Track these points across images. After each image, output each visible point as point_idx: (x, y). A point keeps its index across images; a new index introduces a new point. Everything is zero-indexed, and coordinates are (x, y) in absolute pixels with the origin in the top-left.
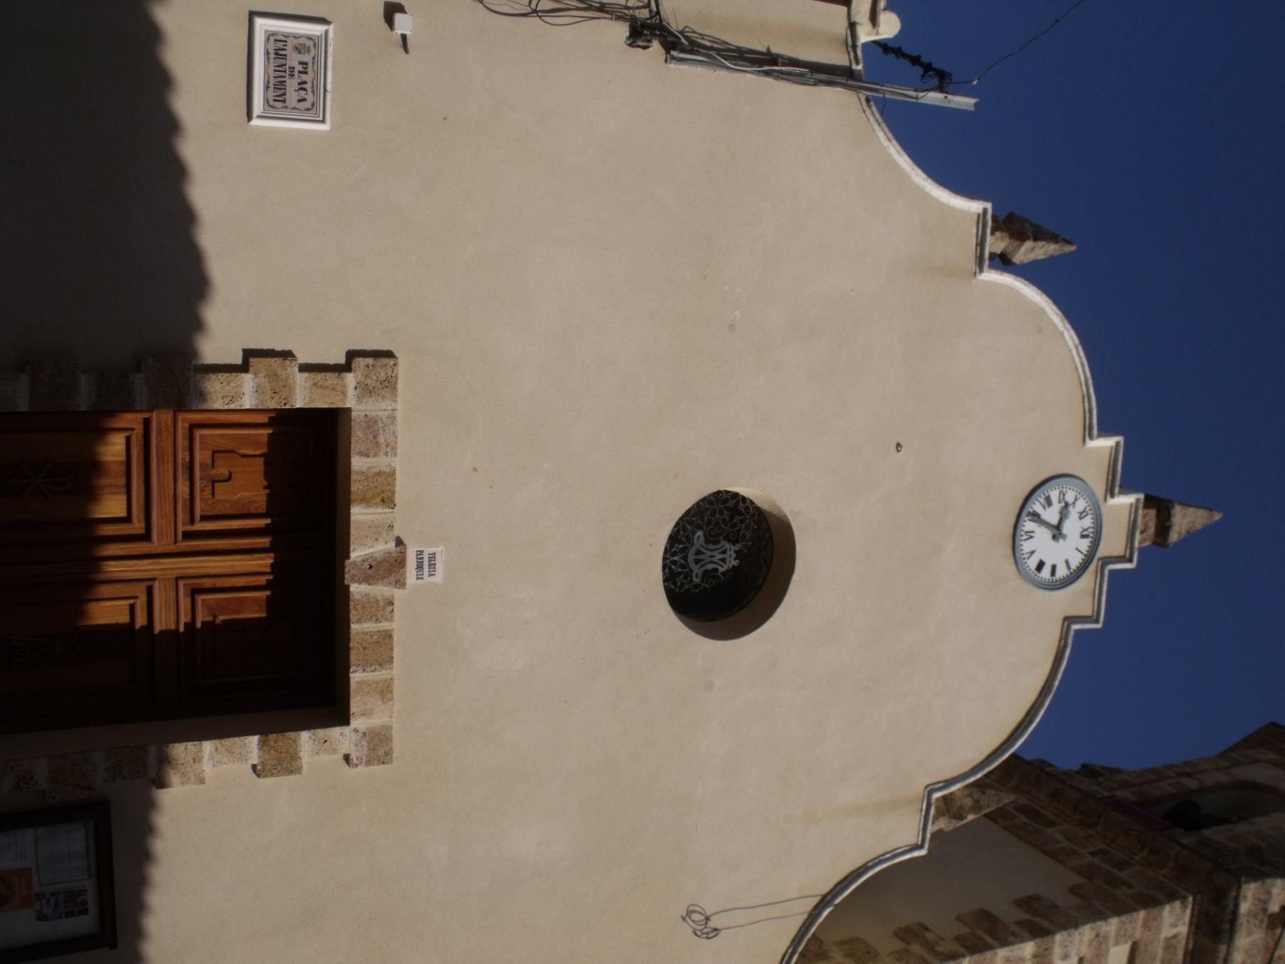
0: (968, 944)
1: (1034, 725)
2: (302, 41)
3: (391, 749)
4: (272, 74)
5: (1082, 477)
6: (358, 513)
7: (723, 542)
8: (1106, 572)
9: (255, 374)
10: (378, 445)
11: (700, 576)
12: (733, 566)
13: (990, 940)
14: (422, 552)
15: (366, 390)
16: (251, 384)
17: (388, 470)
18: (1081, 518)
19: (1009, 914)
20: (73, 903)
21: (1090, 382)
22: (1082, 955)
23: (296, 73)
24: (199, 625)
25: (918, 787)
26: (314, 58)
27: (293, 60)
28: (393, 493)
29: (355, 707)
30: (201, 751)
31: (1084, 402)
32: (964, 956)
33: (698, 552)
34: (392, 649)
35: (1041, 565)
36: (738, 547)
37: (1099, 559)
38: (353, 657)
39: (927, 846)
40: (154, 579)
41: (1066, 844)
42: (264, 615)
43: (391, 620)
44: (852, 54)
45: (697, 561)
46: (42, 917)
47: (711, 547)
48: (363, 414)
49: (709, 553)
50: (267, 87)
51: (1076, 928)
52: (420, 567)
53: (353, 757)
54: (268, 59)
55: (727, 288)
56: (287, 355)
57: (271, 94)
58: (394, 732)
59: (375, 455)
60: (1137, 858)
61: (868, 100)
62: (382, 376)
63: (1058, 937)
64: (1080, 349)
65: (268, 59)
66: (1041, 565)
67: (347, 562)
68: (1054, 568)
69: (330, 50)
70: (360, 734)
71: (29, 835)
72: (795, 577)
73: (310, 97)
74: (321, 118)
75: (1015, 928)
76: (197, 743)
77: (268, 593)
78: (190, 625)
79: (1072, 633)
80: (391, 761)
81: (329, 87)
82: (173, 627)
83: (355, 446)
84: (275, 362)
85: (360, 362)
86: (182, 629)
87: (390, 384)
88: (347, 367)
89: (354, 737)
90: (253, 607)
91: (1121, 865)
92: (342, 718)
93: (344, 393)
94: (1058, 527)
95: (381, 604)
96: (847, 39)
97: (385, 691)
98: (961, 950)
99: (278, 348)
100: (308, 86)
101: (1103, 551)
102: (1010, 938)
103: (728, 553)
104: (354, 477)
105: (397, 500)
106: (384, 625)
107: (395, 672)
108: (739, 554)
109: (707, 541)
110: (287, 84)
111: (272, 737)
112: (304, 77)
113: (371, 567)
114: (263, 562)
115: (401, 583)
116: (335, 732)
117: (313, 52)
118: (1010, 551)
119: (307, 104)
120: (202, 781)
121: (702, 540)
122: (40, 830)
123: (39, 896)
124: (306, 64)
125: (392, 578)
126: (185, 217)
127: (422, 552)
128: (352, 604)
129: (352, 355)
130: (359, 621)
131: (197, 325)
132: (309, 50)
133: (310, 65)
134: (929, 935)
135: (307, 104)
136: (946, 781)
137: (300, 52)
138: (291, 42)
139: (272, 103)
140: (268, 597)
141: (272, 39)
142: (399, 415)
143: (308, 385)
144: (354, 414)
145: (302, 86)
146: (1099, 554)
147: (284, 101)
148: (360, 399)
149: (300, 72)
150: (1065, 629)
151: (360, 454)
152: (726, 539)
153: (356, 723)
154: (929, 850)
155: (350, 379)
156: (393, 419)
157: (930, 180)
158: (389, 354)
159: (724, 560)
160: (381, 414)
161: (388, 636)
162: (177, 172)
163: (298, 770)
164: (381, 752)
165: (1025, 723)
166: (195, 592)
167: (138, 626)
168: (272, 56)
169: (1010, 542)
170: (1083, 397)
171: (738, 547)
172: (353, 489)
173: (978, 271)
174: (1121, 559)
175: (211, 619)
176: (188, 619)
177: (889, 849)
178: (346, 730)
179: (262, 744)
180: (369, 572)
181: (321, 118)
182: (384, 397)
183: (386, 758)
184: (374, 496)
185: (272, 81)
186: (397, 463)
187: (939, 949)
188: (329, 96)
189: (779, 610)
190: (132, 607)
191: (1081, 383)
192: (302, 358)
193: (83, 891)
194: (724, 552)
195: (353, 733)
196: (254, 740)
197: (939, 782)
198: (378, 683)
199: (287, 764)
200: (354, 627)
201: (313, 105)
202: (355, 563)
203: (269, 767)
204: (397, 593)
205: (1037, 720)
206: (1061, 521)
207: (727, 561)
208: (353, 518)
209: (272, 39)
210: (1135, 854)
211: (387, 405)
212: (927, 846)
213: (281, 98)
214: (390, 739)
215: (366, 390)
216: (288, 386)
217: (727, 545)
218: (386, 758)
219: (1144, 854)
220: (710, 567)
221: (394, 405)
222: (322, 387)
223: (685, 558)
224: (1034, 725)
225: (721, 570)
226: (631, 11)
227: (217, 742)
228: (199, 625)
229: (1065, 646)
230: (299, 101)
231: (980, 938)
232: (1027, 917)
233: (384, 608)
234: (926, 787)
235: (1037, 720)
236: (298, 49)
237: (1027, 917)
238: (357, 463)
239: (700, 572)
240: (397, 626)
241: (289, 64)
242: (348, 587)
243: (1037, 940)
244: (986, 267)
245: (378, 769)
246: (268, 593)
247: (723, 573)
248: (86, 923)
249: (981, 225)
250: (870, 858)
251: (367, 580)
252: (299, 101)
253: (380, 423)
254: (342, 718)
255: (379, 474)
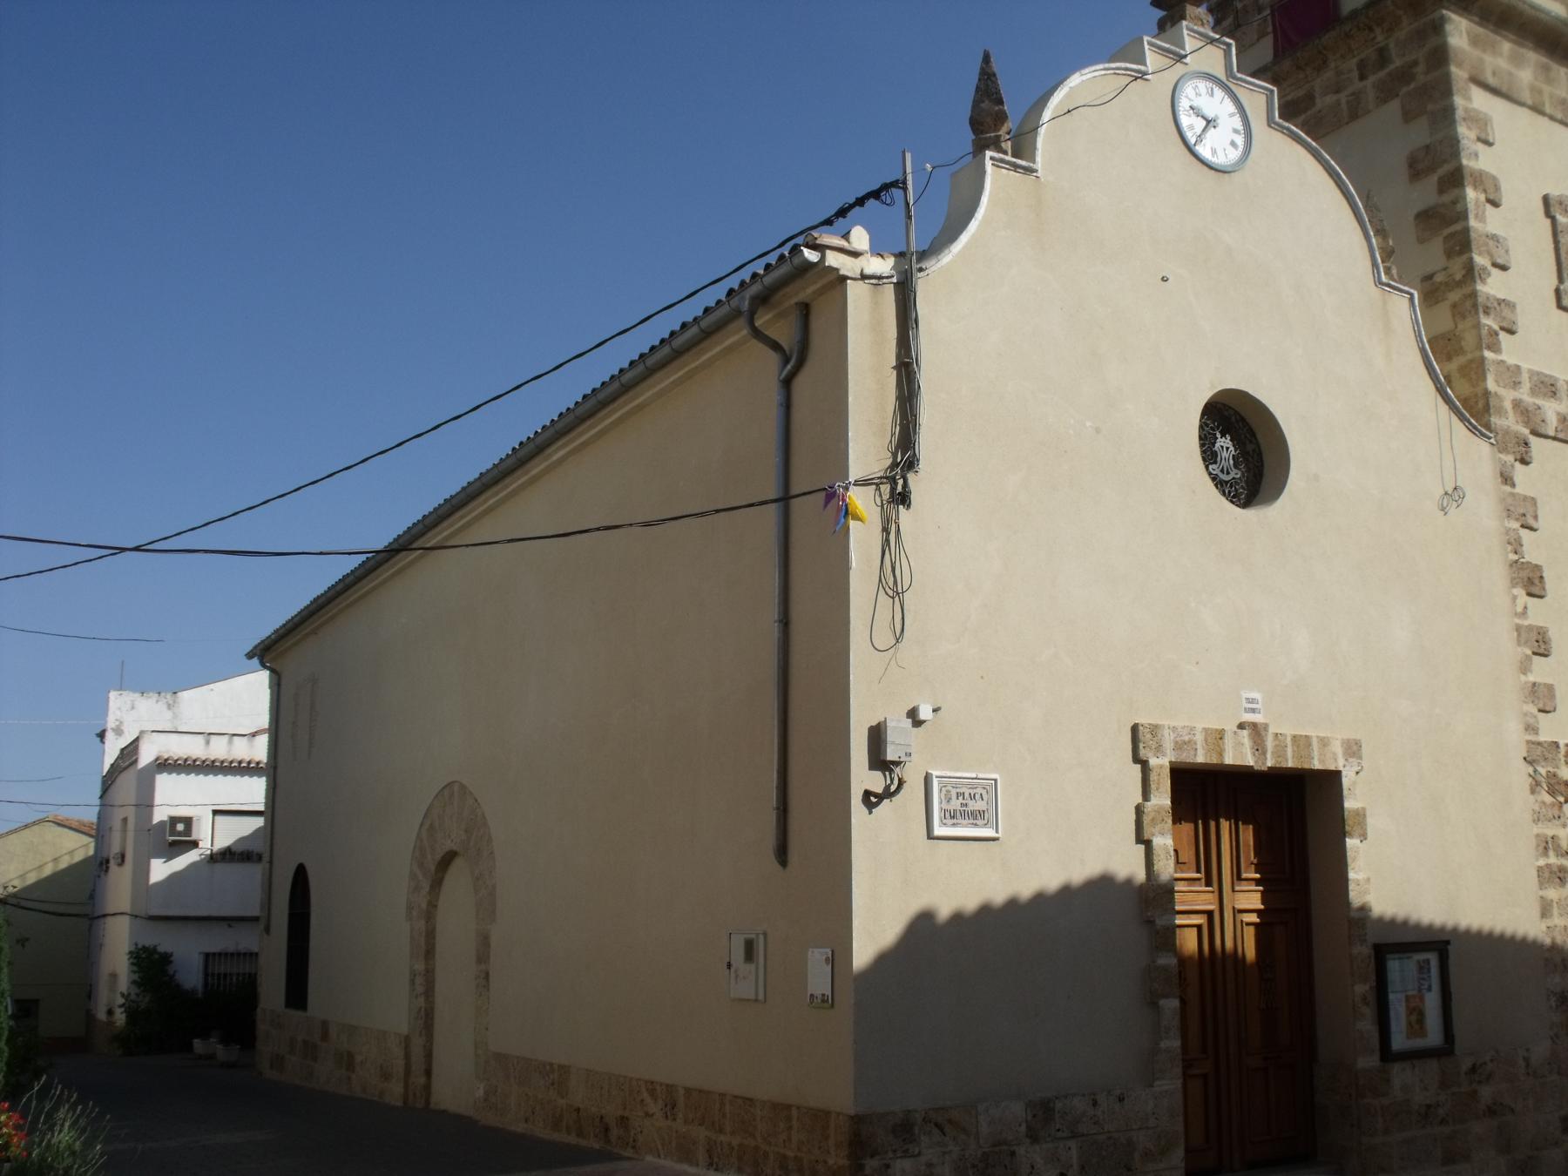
0: (1458, 248)
1: (1341, 173)
2: (943, 798)
3: (1354, 740)
4: (966, 821)
5: (1172, 88)
6: (1229, 760)
7: (1216, 448)
8: (1239, 75)
9: (1153, 835)
10: (1189, 742)
11: (1237, 471)
12: (1231, 440)
13: (1457, 227)
14: (1245, 709)
15: (1159, 750)
16: (1159, 838)
17: (1204, 734)
18: (1200, 95)
19: (1426, 194)
20: (1423, 967)
21: (1107, 65)
22: (1475, 138)
23: (964, 802)
24: (1258, 876)
25: (1375, 292)
26: (953, 787)
27: (956, 804)
28: (1217, 730)
29: (1332, 768)
30: (1354, 880)
31: (1119, 74)
32: (1471, 260)
33: (1222, 471)
34: (1301, 736)
35: (1233, 144)
36: (1218, 435)
37: (1227, 80)
38: (1306, 766)
39: (1412, 291)
40: (1234, 908)
41: (1343, 97)
42: (1251, 826)
43: (1285, 736)
44: (885, 281)
45: (1228, 473)
46: (1430, 989)
47: (1219, 459)
48: (1173, 752)
49: (1223, 461)
50: (976, 825)
51: (1459, 142)
52: (1253, 711)
53: (1357, 769)
54: (958, 824)
55: (1071, 432)
56: (1139, 810)
57: (979, 822)
58: (1345, 737)
59: (1196, 744)
60: (1380, 38)
61: (921, 270)
62: (1149, 736)
63: (1465, 162)
64: (1083, 72)
65: (958, 824)
66: (1233, 144)
67: (1256, 768)
68: (1236, 131)
69: (949, 774)
70: (1347, 764)
71: (1392, 997)
72: (1251, 392)
73: (979, 791)
74: (993, 782)
75: (1446, 198)
76: (1350, 882)
77: (1240, 823)
78: (1258, 882)
79: (1281, 121)
80: (1359, 740)
81: (974, 776)
82: (1259, 895)
83: (1190, 760)
84: (1146, 820)
85: (1143, 753)
86: (1261, 888)
87: (1154, 729)
88: (1144, 764)
89: (1347, 768)
90: (1247, 834)
91: (1383, 57)
92: (1336, 775)
93: (1161, 767)
94: (1208, 122)
95: (1277, 743)
96: (872, 284)
97: (1324, 742)
98: (1464, 257)
99: (1134, 817)
100: (972, 792)
101: (1220, 73)
102: (1459, 207)
103: (1222, 444)
104: (1209, 762)
105: (1219, 727)
106: (1289, 739)
107: (1313, 734)
108: (1223, 435)
109: (1215, 462)
110: (972, 809)
111: (1347, 828)
112: (967, 795)
113: (1257, 750)
114: (1225, 825)
115: (1266, 727)
116: (1346, 782)
117: (950, 788)
118: (1226, 175)
119: (984, 792)
120: (1368, 880)
121: (1214, 466)
122: (1390, 990)
123: (1420, 990)
124: (958, 793)
125: (1263, 733)
126: (1066, 891)
127: (1245, 709)
128: (1277, 766)
129: (1137, 759)
130: (1287, 760)
131: (1129, 882)
132: (948, 791)
133: (958, 790)
134: (1439, 278)
135: (984, 792)
136: (1373, 266)
137: (951, 799)
138: (945, 806)
139: (986, 822)
140: (1243, 824)
141: (944, 821)
142: (1173, 724)
143: (1158, 794)
144: (1173, 760)
145: (972, 797)
146: (1223, 78)
147: (984, 811)
148: (1164, 755)
149: (964, 798)
150: (1276, 127)
151: (1195, 755)
152: (1214, 444)
153: (1341, 769)
154: (1416, 289)
155: (1153, 762)
156: (1174, 729)
157: (976, 215)
158: (1135, 729)
159: (1227, 448)
160: (1172, 738)
161: (1294, 737)
162: (1040, 898)
163: (1364, 809)
164: (1355, 748)
165: (1338, 181)
166: (1239, 878)
167: (1258, 920)
168: (955, 821)
169: (1221, 174)
170: (1115, 74)
171: (1218, 435)
172: (1215, 762)
173: (1035, 174)
174: (1227, 54)
175: (1253, 866)
176: (1254, 882)
177: (1411, 325)
178: (1344, 774)
179: (1351, 836)
180: (1260, 751)
181: (993, 782)
182: (1163, 736)
183: (1358, 743)
184: (1219, 746)
185: (971, 821)
186: (1200, 726)
187: (1458, 277)
188: (980, 776)
189: (1271, 409)
190: (1248, 924)
191: (1105, 75)
192: (1140, 800)
193: (1418, 962)
194: (1222, 447)
195: (1346, 769)
196: (1348, 840)
197: (1373, 271)
198: (1320, 748)
199: (1361, 815)
200: (1290, 764)
201: (984, 788)
202: (1256, 762)
203: (1362, 832)
204: (1272, 730)
205: (1338, 168)
206: (1203, 117)
207: (1228, 446)
208: (1231, 763)
209: (944, 821)
210: (1374, 38)
211: (1166, 732)
212: (1412, 291)
213: (981, 813)
214: (1348, 740)
215: (1159, 750)
216: (1159, 810)
217: (1217, 445)
218: (1358, 743)
219: (1378, 31)
220: (1231, 462)
221: (1167, 728)
222: (1158, 784)
223: (1227, 482)
224: (1341, 173)
225: (1233, 452)
226: (884, 502)
227: (1349, 868)
228: (1258, 876)
229: (1288, 129)
230: (982, 799)
231: (1452, 235)
232: (1434, 178)
233: (1280, 741)
234: (1376, 285)
235: (1338, 168)
236: (949, 800)
237: (1434, 178)
238: (1200, 759)
239: (1235, 471)
240: (1288, 730)
241: (959, 808)
242: (1268, 767)
243: (1466, 184)
244: (1034, 166)
245: (1365, 751)
246: (1240, 823)
247: (1235, 451)
248: (1433, 958)
249: (1000, 164)
250: (1416, 343)
251: (1264, 753)
252: (982, 799)
253: (1177, 739)
254: (1336, 775)
255: (1206, 740)
